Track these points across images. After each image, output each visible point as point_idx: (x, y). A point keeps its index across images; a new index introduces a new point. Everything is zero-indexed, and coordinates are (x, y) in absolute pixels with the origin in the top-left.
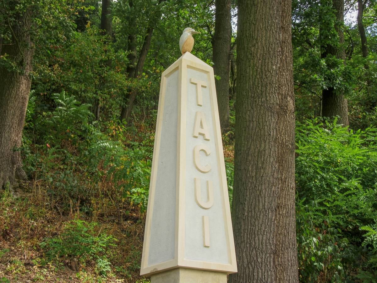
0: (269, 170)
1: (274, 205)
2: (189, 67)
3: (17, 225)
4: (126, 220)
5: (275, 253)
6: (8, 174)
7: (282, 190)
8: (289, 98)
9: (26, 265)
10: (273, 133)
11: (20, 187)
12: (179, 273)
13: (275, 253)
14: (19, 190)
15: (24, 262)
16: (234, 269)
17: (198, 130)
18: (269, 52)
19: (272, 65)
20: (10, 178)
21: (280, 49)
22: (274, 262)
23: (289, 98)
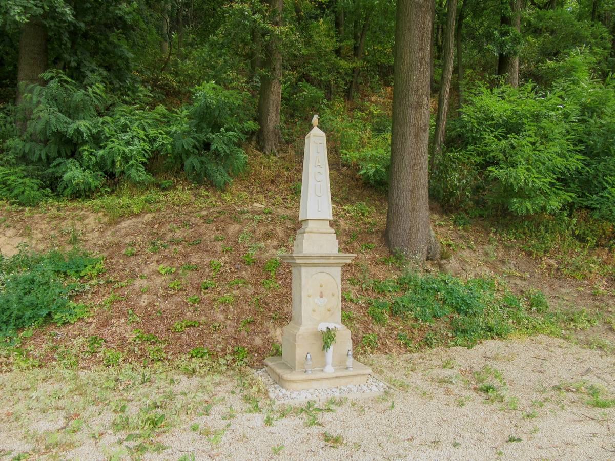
0: (409, 144)
1: (412, 164)
2: (314, 136)
3: (279, 176)
4: (344, 167)
5: (411, 191)
6: (273, 142)
7: (417, 155)
8: (424, 97)
9: (283, 199)
10: (412, 121)
11: (281, 149)
12: (308, 224)
13: (411, 191)
14: (281, 152)
15: (282, 197)
16: (331, 218)
17: (317, 164)
18: (411, 67)
19: (413, 76)
20: (275, 144)
21: (419, 64)
22: (411, 196)
23: (424, 97)
